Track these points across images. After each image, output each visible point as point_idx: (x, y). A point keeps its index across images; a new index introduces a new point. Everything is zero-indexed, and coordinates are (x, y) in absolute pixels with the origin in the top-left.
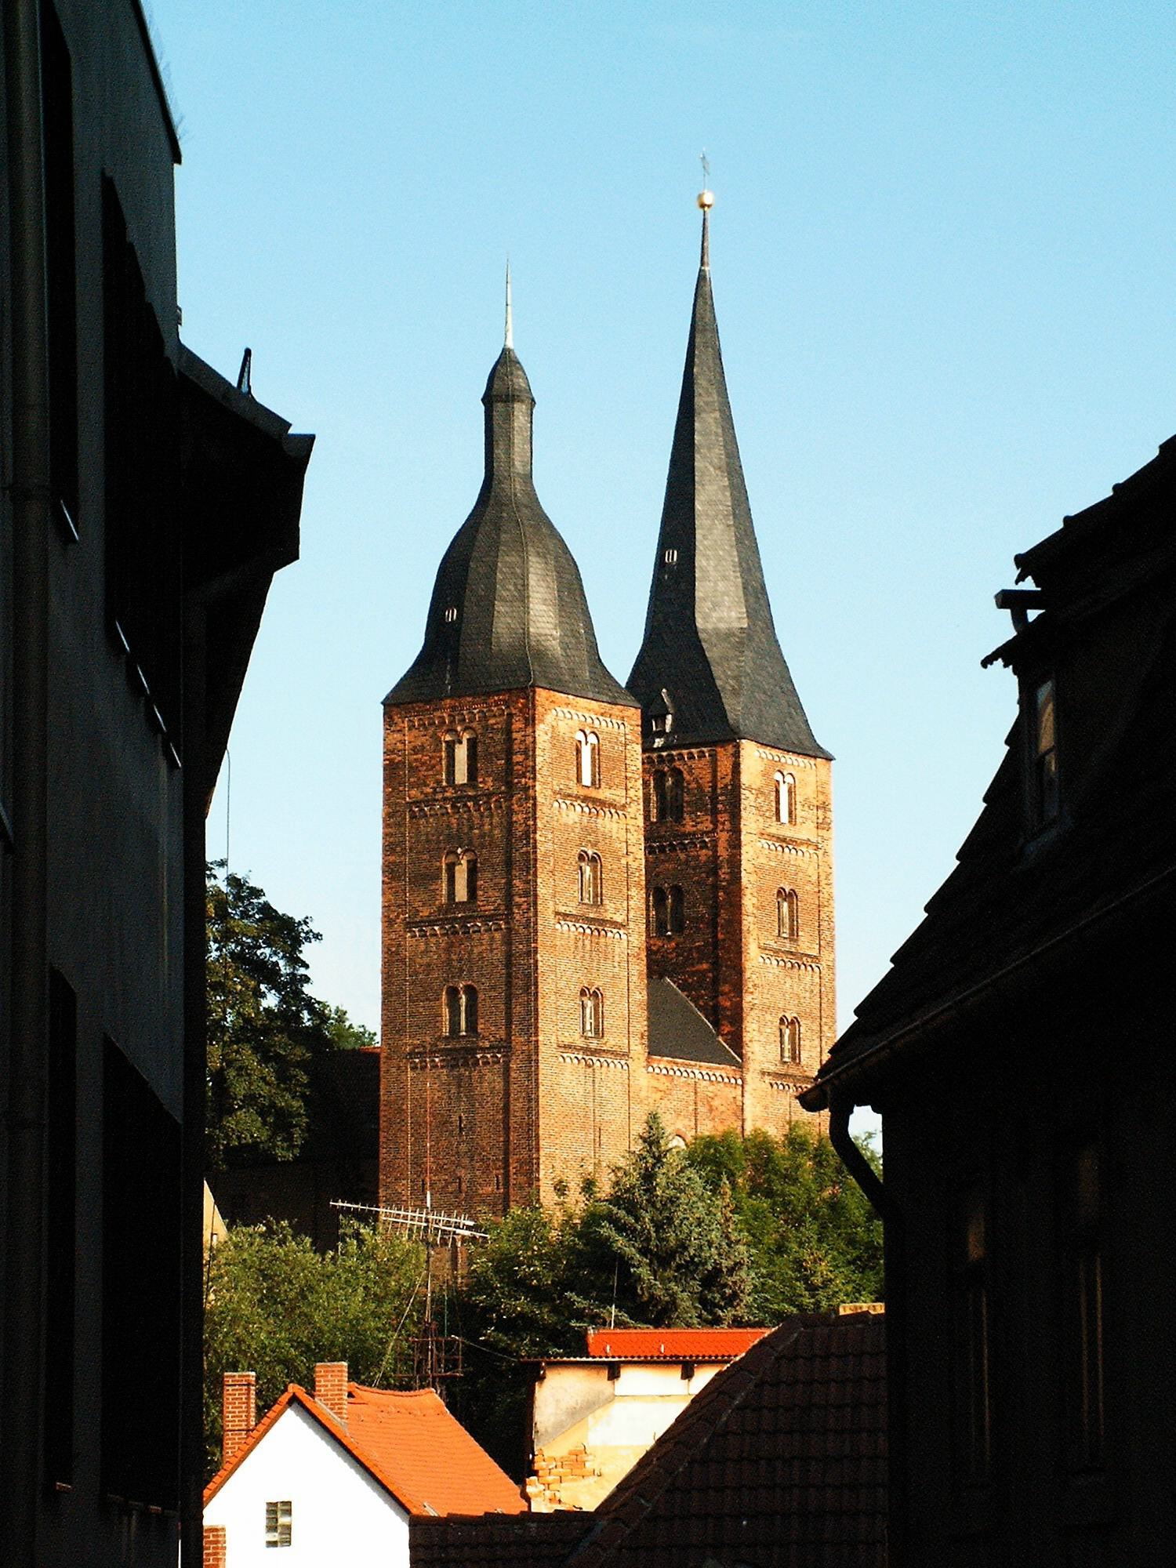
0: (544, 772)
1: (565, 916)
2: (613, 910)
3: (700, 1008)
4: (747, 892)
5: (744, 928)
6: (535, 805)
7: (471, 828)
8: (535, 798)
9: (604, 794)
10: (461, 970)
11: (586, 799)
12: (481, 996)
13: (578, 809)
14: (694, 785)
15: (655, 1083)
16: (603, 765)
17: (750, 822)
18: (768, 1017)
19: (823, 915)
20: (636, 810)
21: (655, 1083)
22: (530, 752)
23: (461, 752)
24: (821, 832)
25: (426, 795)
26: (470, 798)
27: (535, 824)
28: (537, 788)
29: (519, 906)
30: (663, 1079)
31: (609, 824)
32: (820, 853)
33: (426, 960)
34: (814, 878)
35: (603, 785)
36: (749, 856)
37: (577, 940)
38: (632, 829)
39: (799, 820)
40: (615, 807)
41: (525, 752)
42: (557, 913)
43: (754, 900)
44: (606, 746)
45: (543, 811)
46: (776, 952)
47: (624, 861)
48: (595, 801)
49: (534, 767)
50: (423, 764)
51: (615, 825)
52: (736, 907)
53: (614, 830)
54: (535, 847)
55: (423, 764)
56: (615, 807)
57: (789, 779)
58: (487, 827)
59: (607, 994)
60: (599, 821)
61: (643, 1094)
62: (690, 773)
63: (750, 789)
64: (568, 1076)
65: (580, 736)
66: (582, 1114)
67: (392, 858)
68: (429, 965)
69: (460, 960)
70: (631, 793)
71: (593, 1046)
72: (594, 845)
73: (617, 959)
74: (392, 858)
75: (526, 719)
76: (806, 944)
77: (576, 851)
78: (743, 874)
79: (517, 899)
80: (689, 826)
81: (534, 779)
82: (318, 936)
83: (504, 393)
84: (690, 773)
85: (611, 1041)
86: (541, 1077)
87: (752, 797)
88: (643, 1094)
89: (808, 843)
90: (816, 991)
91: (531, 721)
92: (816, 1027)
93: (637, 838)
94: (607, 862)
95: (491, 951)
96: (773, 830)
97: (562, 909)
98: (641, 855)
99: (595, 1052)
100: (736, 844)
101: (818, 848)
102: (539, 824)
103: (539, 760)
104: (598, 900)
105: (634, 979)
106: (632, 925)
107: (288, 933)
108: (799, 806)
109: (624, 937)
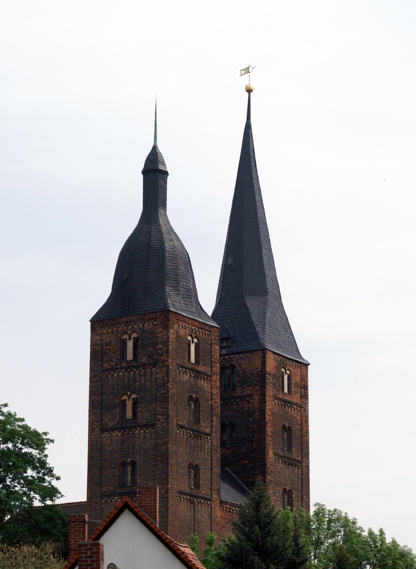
0: (173, 353)
1: (182, 427)
2: (205, 427)
3: (244, 483)
4: (269, 425)
5: (267, 443)
6: (168, 369)
7: (135, 382)
8: (168, 366)
9: (201, 368)
10: (129, 453)
11: (192, 370)
12: (138, 466)
13: (188, 374)
14: (242, 373)
15: (223, 515)
16: (201, 354)
17: (270, 391)
18: (278, 488)
19: (303, 441)
20: (216, 378)
21: (223, 515)
22: (166, 343)
23: (130, 345)
24: (303, 400)
25: (112, 366)
26: (134, 367)
27: (168, 379)
28: (170, 361)
29: (159, 420)
30: (227, 513)
31: (204, 384)
32: (303, 410)
33: (111, 448)
34: (299, 422)
35: (201, 364)
36: (269, 407)
37: (187, 439)
38: (214, 387)
39: (293, 392)
40: (206, 375)
41: (163, 343)
42: (178, 425)
43: (272, 429)
44: (202, 345)
45: (172, 373)
46: (282, 457)
47: (210, 403)
48: (197, 371)
49: (168, 351)
50: (110, 351)
51: (206, 384)
52: (263, 432)
53: (206, 387)
54: (168, 390)
55: (110, 351)
56: (206, 375)
57: (288, 372)
58: (143, 381)
59: (202, 468)
60: (199, 381)
61: (218, 520)
62: (240, 366)
63: (270, 374)
64: (182, 508)
65: (190, 338)
66: (189, 527)
67: (94, 398)
68: (112, 450)
69: (128, 448)
70: (214, 369)
71: (194, 493)
72: (197, 393)
73: (206, 450)
74: (94, 398)
75: (164, 327)
76: (296, 455)
77: (187, 395)
78: (267, 416)
79: (158, 417)
80: (239, 393)
81: (168, 356)
82: (52, 441)
83: (154, 174)
84: (240, 366)
85: (204, 491)
86: (170, 506)
87: (271, 379)
88: (218, 520)
89: (296, 404)
90: (300, 477)
91: (166, 328)
92: (300, 495)
93: (216, 391)
94: (202, 402)
95: (144, 443)
96: (281, 396)
97: (180, 423)
98: (218, 400)
99: (195, 497)
100: (263, 402)
101: (301, 407)
102: (170, 379)
103: (170, 347)
104: (197, 420)
105: (214, 462)
106: (214, 435)
107: (38, 440)
108: (293, 386)
109: (209, 440)
